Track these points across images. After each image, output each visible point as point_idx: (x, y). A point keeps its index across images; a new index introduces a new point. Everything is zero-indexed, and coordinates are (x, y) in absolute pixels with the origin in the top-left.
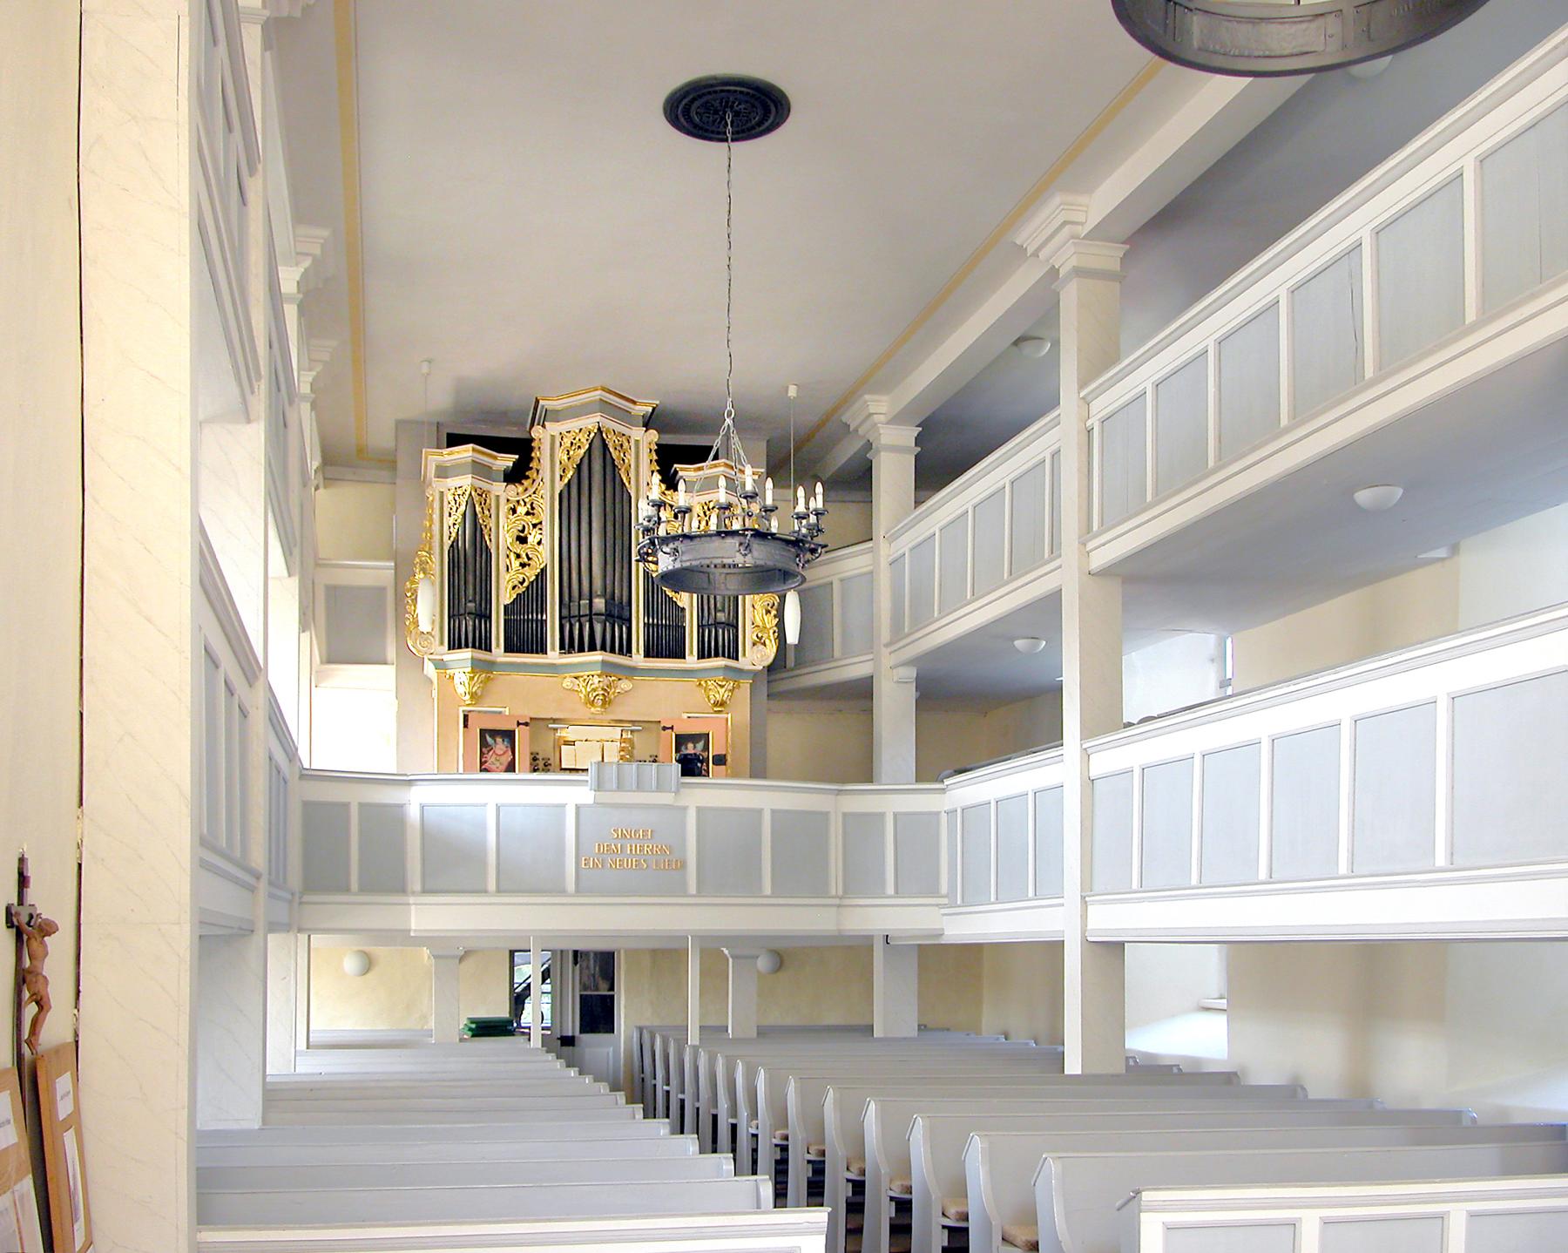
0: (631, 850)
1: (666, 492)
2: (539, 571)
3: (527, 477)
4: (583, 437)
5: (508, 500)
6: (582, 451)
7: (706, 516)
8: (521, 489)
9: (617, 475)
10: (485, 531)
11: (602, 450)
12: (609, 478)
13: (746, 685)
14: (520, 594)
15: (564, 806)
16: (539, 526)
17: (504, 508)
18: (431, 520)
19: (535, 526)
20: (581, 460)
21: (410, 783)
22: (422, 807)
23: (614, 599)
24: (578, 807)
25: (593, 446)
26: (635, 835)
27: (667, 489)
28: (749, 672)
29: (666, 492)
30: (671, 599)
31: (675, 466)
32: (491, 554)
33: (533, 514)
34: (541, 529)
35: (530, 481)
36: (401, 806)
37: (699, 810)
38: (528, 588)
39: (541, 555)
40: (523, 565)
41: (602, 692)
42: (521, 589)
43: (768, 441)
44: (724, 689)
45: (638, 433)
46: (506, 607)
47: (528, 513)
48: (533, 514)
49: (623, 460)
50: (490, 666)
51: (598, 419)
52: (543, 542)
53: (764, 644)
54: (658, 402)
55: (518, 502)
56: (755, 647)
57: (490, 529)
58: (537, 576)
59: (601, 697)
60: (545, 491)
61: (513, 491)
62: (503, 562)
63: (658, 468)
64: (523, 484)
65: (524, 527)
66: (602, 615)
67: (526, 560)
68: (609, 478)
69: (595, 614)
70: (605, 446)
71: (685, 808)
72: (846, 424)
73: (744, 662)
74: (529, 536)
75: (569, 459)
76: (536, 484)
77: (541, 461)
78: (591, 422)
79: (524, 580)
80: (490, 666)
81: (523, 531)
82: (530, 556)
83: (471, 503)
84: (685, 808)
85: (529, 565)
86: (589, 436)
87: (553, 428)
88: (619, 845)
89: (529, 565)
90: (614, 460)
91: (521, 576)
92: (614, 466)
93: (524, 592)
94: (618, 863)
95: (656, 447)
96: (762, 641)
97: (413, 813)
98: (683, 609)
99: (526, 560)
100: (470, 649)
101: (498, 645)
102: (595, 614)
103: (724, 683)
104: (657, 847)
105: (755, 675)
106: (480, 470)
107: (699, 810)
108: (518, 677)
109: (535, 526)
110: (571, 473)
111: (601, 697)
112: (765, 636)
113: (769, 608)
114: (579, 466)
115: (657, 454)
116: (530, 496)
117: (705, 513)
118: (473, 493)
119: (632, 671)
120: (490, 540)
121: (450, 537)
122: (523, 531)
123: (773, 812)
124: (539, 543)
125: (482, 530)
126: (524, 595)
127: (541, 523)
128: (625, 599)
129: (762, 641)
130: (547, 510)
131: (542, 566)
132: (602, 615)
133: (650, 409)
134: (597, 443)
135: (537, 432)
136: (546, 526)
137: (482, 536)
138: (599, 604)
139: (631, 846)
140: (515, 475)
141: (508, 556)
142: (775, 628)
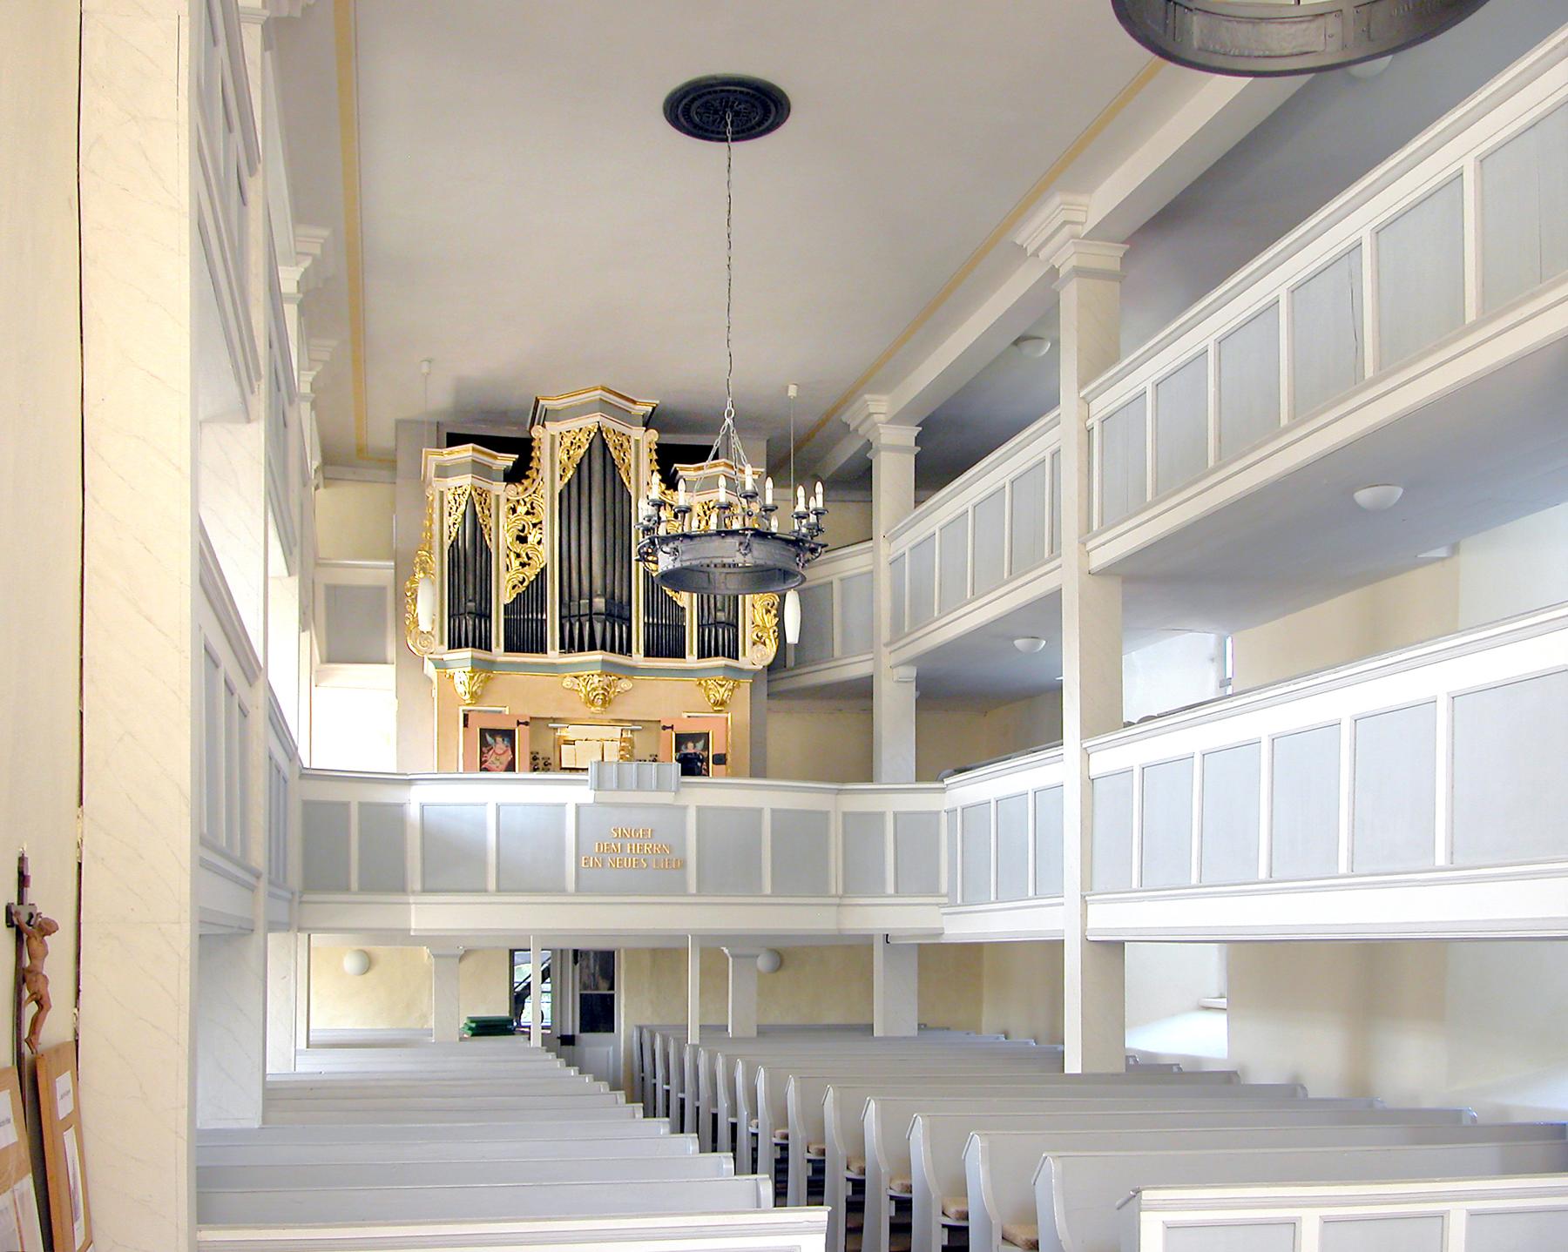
0: (631, 849)
1: (666, 492)
2: (539, 570)
3: (527, 477)
4: (583, 437)
5: (508, 500)
6: (582, 451)
7: (706, 515)
8: (521, 488)
9: (617, 475)
10: (485, 531)
11: (602, 450)
12: (609, 477)
13: (746, 684)
14: (520, 594)
15: (564, 805)
16: (539, 526)
17: (504, 508)
18: (431, 520)
19: (535, 525)
20: (581, 459)
21: (410, 782)
22: (422, 807)
23: (614, 598)
24: (578, 807)
25: (593, 445)
26: (635, 834)
27: (667, 488)
28: (749, 671)
29: (666, 492)
30: (671, 598)
31: (675, 465)
32: (491, 553)
33: (533, 514)
34: (541, 529)
35: (530, 480)
36: (401, 805)
37: (699, 809)
38: (528, 587)
39: (541, 555)
40: (523, 565)
41: (602, 692)
42: (521, 589)
43: (768, 441)
44: (724, 689)
45: (638, 433)
46: (506, 606)
47: (528, 513)
48: (533, 514)
49: (623, 460)
50: (490, 666)
51: (598, 419)
52: (543, 541)
53: (764, 644)
54: (658, 402)
55: (518, 501)
56: (755, 646)
57: (490, 529)
58: (537, 576)
59: (601, 697)
60: (545, 490)
61: (513, 490)
62: (503, 561)
63: (658, 468)
64: (523, 484)
65: (524, 526)
66: (602, 614)
67: (526, 560)
68: (609, 477)
69: (595, 614)
70: (605, 446)
71: (685, 808)
72: (846, 423)
73: (744, 662)
74: (529, 535)
75: (569, 458)
76: (536, 484)
77: (541, 460)
78: (591, 421)
79: (524, 579)
80: (490, 666)
81: (523, 531)
82: (530, 556)
83: (471, 503)
84: (685, 808)
85: (529, 564)
86: (589, 435)
87: (553, 428)
88: (619, 844)
89: (529, 564)
90: (614, 460)
91: (521, 576)
92: (614, 466)
93: (524, 592)
94: (618, 862)
95: (656, 447)
96: (762, 640)
97: (413, 812)
98: (683, 609)
99: (526, 560)
100: (470, 649)
101: (498, 645)
102: (595, 614)
103: (724, 683)
104: (657, 846)
105: (755, 674)
106: (480, 469)
107: (699, 809)
108: (518, 676)
109: (535, 525)
110: (571, 473)
111: (601, 697)
112: (765, 635)
113: (769, 608)
114: (579, 466)
115: (657, 454)
116: (530, 495)
117: (705, 512)
118: (473, 493)
119: (632, 671)
120: (490, 540)
121: (450, 537)
122: (523, 531)
123: (773, 811)
124: (539, 543)
125: (482, 529)
126: (524, 595)
127: (541, 523)
128: (625, 598)
129: (762, 640)
130: (547, 509)
131: (542, 566)
132: (602, 614)
133: (650, 409)
134: (597, 443)
135: (537, 432)
136: (546, 526)
137: (482, 535)
138: (599, 603)
139: (631, 845)
140: (515, 475)
141: (508, 556)
142: (775, 628)
